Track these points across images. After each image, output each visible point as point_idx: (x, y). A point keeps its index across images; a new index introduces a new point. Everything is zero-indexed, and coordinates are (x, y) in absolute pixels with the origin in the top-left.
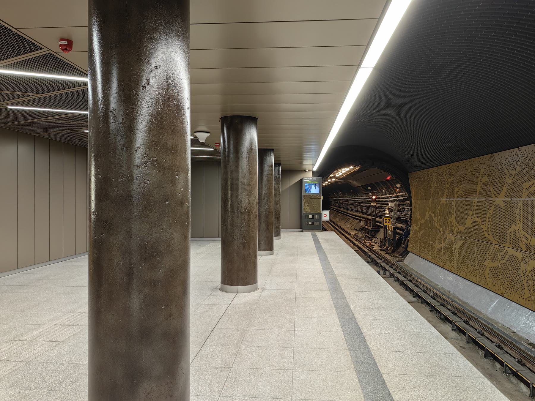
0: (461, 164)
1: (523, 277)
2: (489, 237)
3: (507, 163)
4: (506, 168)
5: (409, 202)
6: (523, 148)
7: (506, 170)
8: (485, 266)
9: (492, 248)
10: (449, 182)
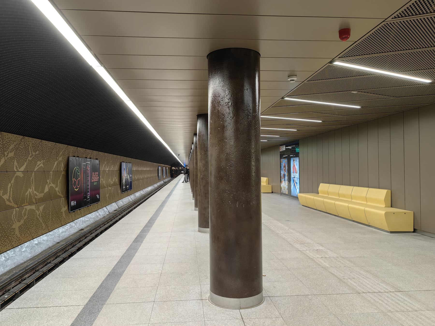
0: (31, 141)
1: (40, 219)
3: (32, 146)
4: (31, 150)
6: (44, 141)
7: (30, 151)
8: (15, 229)
9: (14, 212)
10: (32, 155)
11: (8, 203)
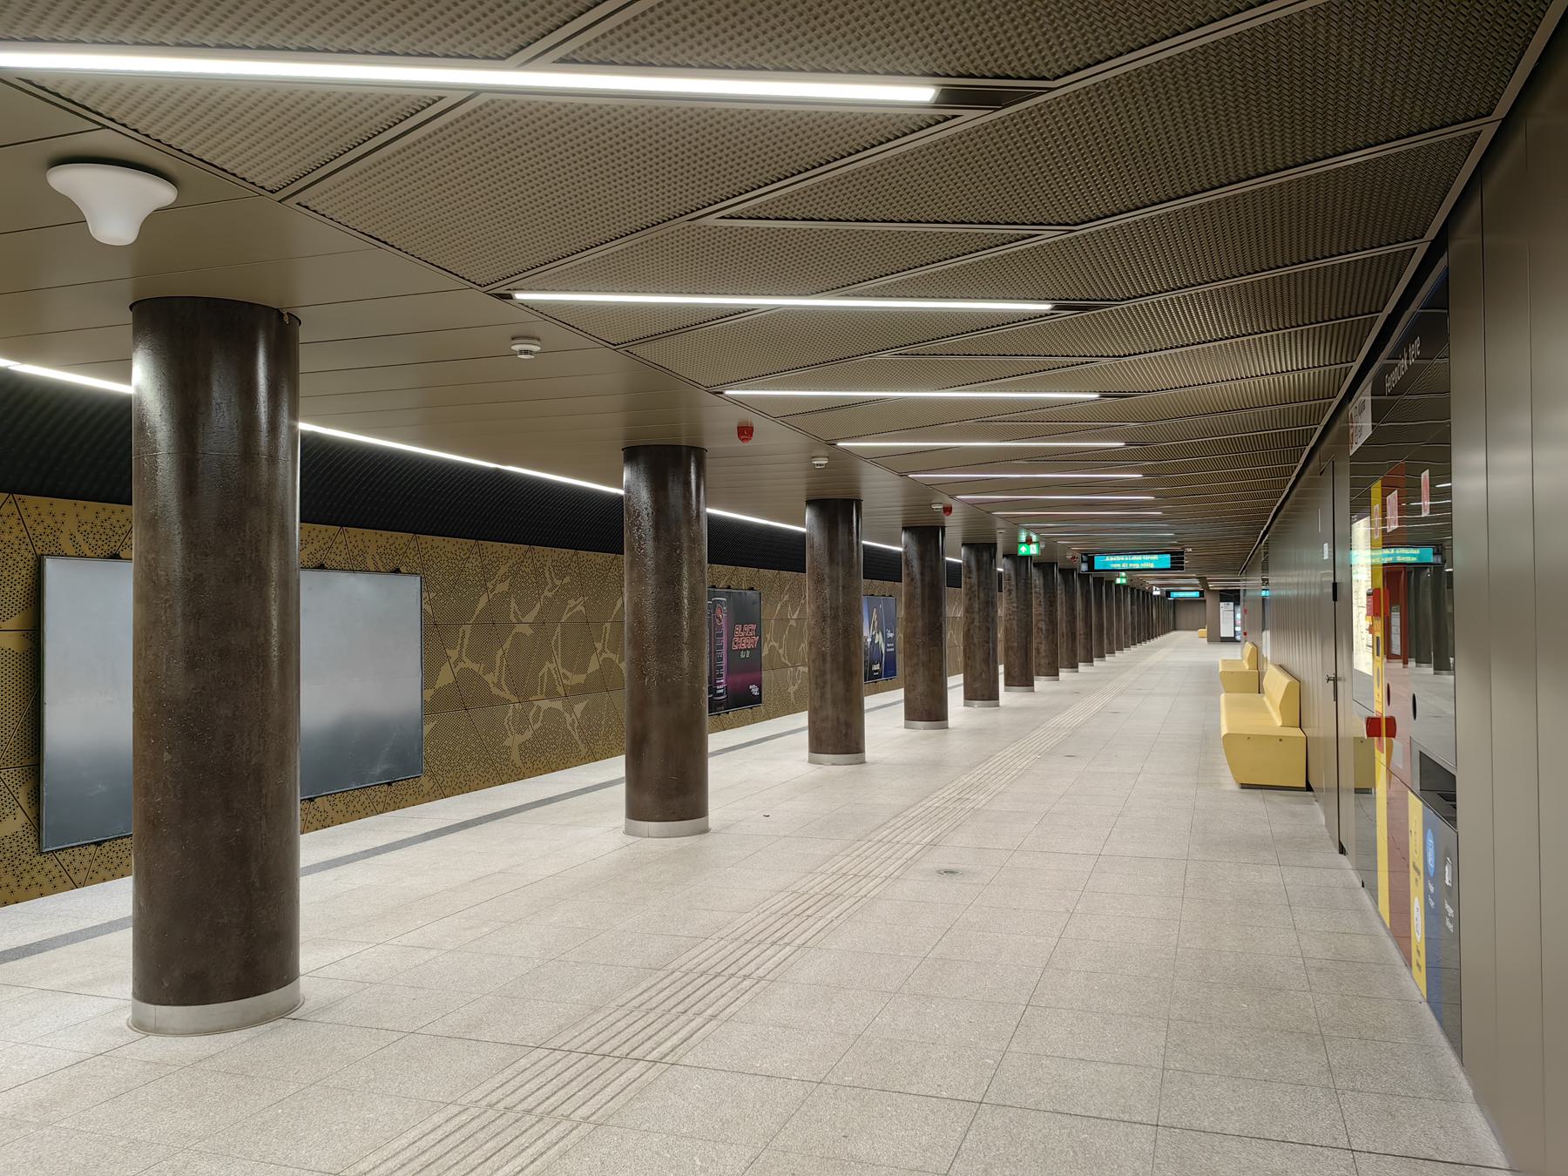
2: (502, 694)
3: (85, 534)
5: (753, 627)
11: (495, 691)
